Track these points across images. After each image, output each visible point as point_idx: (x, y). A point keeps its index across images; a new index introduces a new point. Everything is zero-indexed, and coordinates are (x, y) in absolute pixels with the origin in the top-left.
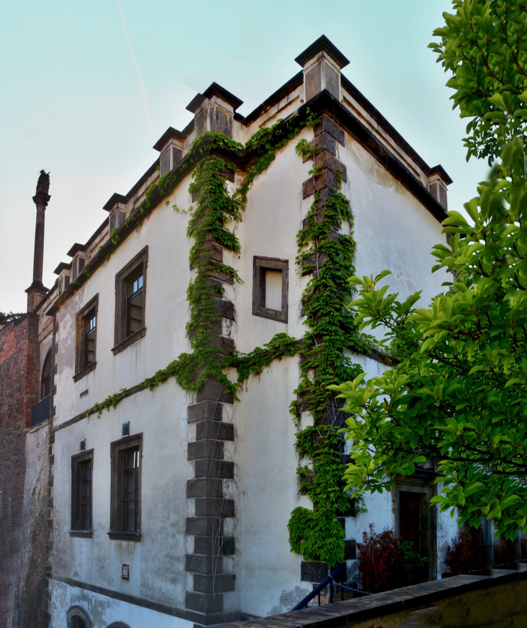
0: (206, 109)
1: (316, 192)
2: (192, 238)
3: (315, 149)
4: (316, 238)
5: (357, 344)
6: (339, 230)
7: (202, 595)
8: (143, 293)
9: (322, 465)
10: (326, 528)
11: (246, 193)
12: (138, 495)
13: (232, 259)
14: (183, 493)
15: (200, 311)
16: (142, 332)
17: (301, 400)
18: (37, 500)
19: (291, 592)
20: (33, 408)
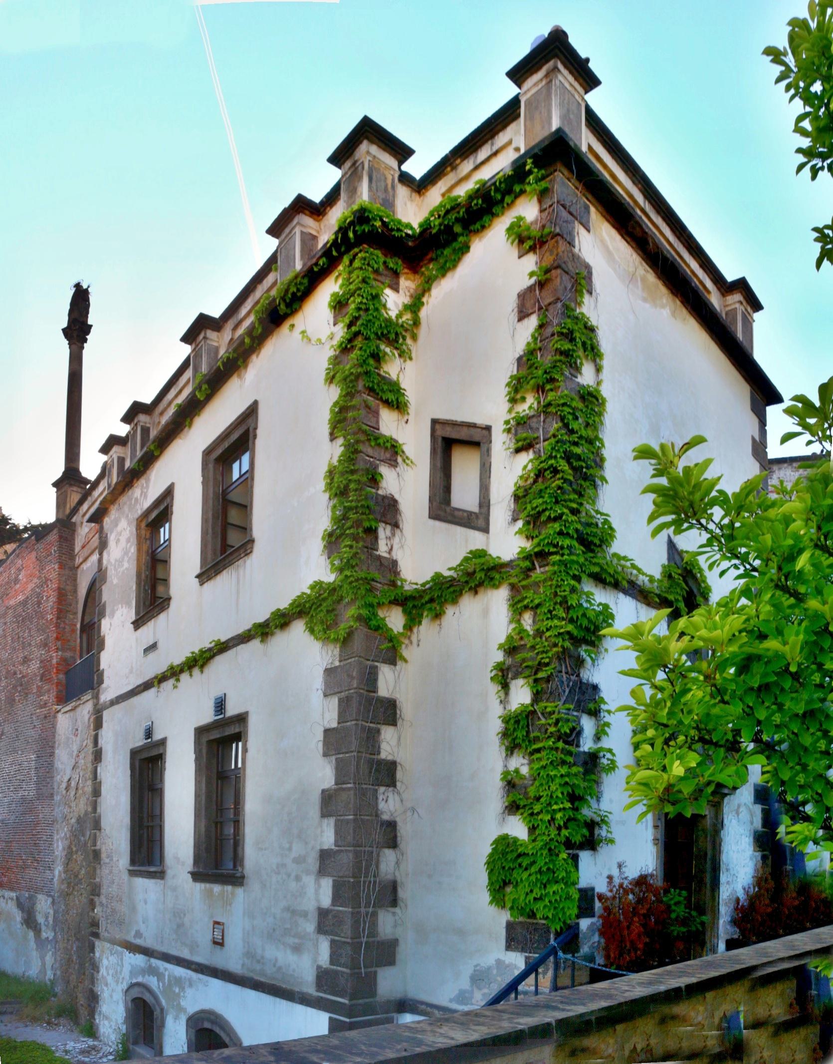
0: (362, 163)
1: (540, 308)
2: (333, 386)
3: (539, 234)
4: (540, 389)
5: (606, 570)
6: (579, 376)
7: (344, 972)
8: (249, 480)
9: (544, 767)
10: (548, 869)
11: (419, 310)
12: (239, 812)
13: (396, 423)
14: (314, 809)
15: (348, 509)
16: (247, 547)
17: (509, 661)
18: (73, 799)
19: (489, 968)
20: (66, 673)
